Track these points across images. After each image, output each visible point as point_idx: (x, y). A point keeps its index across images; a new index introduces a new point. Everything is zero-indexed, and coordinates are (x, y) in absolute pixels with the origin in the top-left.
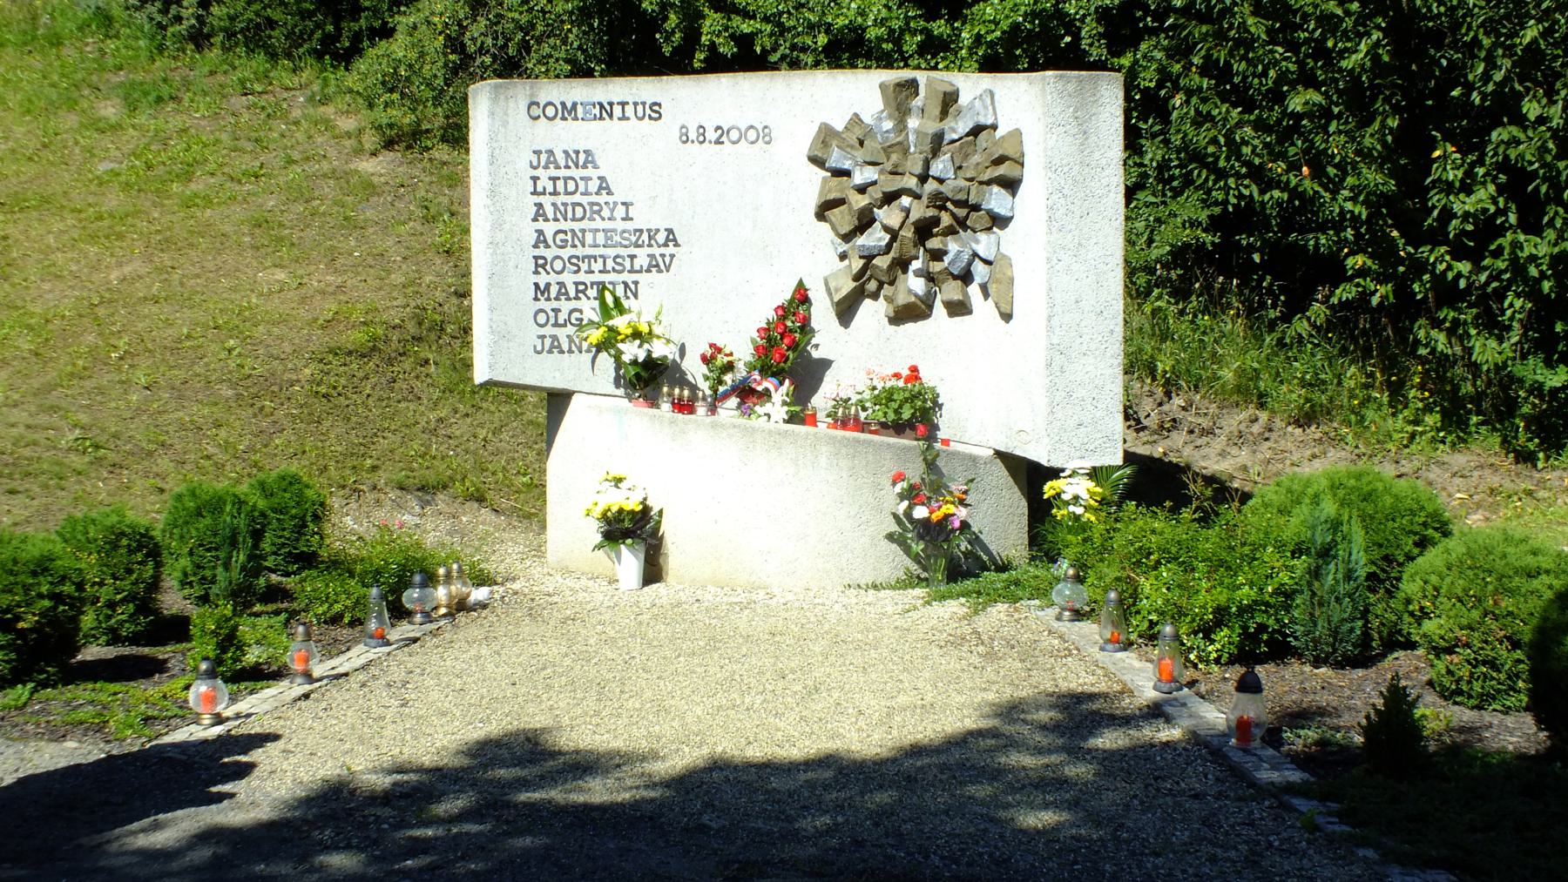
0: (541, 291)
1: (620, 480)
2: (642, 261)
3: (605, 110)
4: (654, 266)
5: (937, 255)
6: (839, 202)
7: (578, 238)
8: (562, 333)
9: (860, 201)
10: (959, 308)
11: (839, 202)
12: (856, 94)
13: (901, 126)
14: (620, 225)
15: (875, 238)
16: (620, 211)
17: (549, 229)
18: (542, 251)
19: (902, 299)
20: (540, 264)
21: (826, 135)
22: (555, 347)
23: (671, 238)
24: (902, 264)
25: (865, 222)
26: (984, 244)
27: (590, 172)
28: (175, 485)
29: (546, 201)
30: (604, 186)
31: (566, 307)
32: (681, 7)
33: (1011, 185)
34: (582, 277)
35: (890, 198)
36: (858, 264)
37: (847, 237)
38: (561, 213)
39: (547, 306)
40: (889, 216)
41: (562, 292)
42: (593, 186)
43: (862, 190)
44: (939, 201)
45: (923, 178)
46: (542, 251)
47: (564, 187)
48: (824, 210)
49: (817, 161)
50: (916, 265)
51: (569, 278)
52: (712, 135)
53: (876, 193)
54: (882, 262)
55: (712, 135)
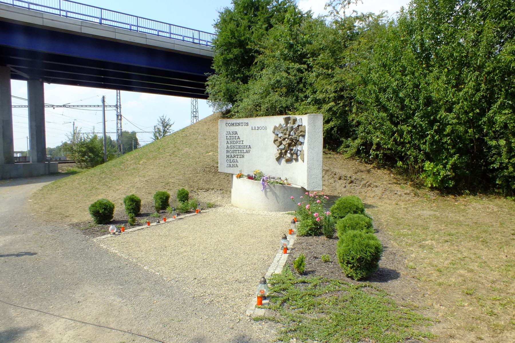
0: (228, 156)
1: (340, 177)
2: (245, 151)
3: (239, 124)
4: (247, 152)
5: (292, 150)
6: (277, 140)
7: (234, 147)
8: (231, 164)
9: (279, 140)
10: (297, 160)
11: (277, 140)
12: (279, 120)
13: (287, 125)
14: (241, 145)
15: (282, 147)
16: (241, 142)
17: (229, 145)
18: (228, 149)
19: (287, 158)
20: (227, 152)
21: (275, 128)
22: (230, 166)
23: (250, 147)
24: (286, 152)
25: (281, 143)
26: (299, 148)
27: (236, 135)
28: (122, 202)
29: (229, 141)
30: (239, 138)
31: (232, 159)
32: (199, 123)
33: (303, 136)
34: (235, 154)
35: (284, 139)
36: (280, 151)
37: (278, 146)
38: (231, 143)
39: (229, 159)
40: (284, 143)
41: (231, 156)
42: (237, 138)
43: (280, 138)
44: (292, 140)
45: (289, 135)
46: (228, 149)
47: (233, 137)
48: (275, 141)
49: (274, 132)
50: (289, 152)
51: (232, 154)
52: (257, 128)
53: (282, 138)
54: (283, 151)
55: (257, 128)
